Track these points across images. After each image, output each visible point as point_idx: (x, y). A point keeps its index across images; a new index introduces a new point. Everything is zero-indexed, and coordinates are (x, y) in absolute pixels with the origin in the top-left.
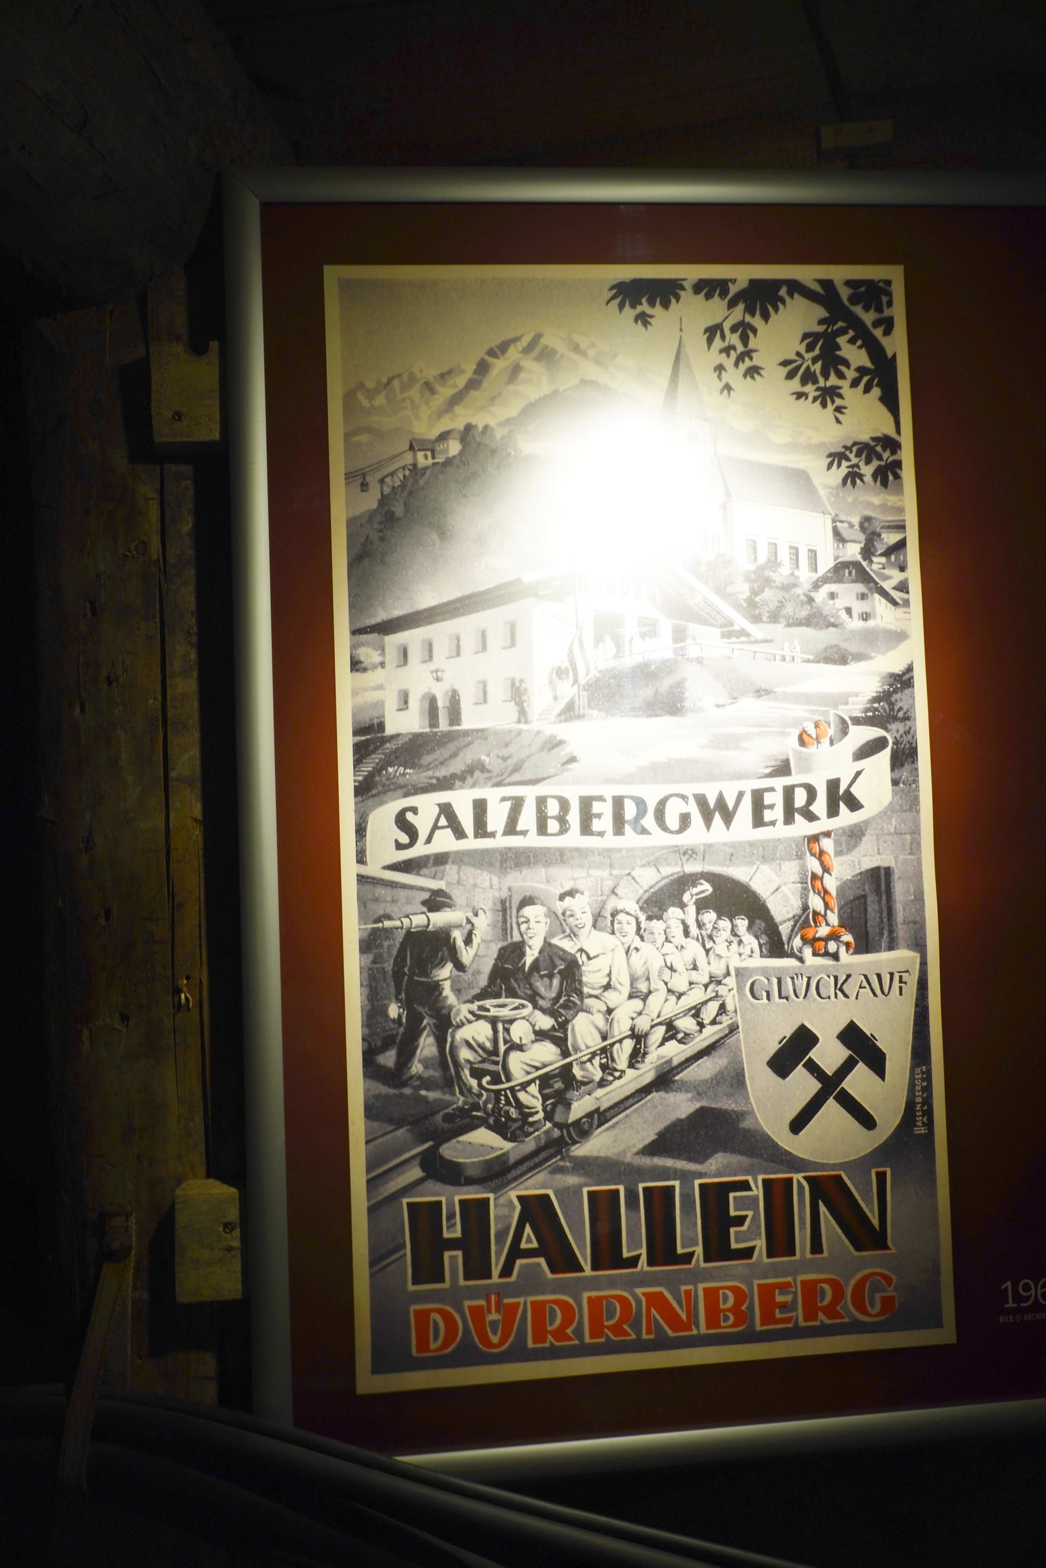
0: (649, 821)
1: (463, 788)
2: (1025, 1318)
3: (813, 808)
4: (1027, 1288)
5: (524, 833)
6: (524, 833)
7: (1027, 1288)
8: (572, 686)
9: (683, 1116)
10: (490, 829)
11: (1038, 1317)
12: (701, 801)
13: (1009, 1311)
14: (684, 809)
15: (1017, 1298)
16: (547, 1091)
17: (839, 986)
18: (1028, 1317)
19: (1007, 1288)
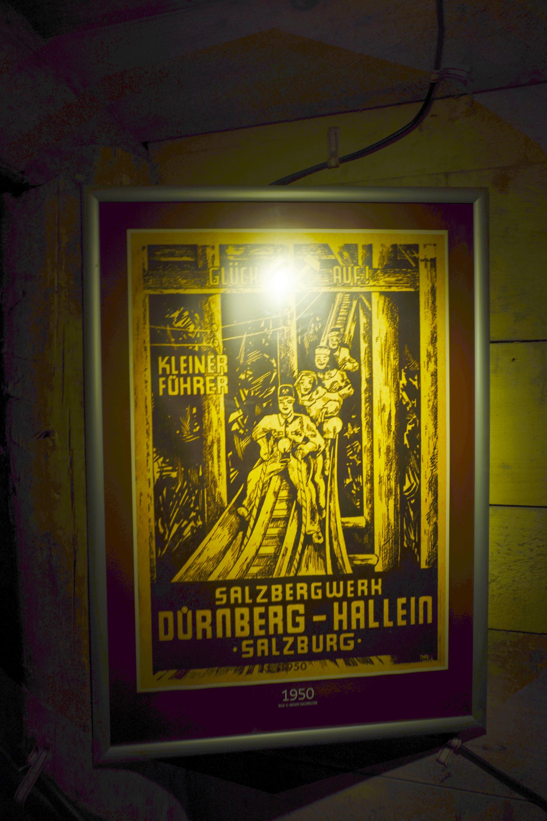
2: (290, 705)
4: (294, 693)
7: (294, 693)
13: (285, 703)
15: (289, 697)
19: (284, 694)
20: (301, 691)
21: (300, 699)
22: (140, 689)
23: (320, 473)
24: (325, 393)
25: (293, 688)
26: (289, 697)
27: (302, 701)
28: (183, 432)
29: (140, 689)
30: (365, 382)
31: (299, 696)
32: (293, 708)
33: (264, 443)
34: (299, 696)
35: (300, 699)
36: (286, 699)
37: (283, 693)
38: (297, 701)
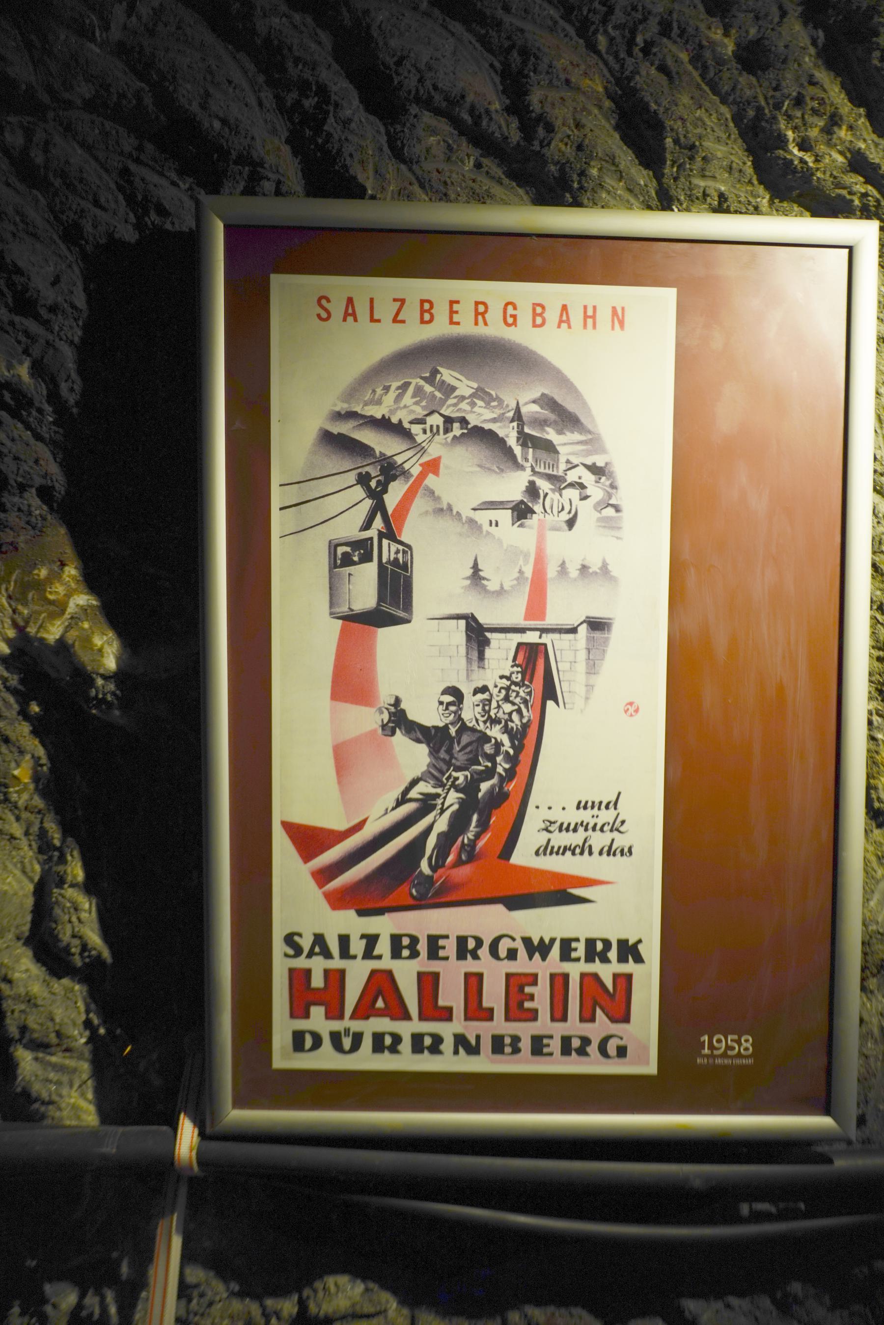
0: (484, 952)
1: (871, 609)
2: (716, 1061)
3: (479, 952)
4: (719, 1041)
5: (379, 957)
6: (379, 957)
7: (719, 1041)
8: (531, 958)
9: (392, 483)
10: (352, 952)
11: (726, 1061)
12: (527, 941)
13: (707, 1056)
14: (512, 945)
15: (711, 1047)
16: (706, 81)
17: (418, 903)
18: (719, 1061)
19: (704, 1041)
20: (732, 1040)
21: (730, 1053)
22: (276, 280)
23: (463, 650)
24: (364, 499)
25: (749, 1034)
26: (711, 1047)
27: (732, 1057)
28: (57, 936)
29: (276, 280)
30: (881, 139)
31: (728, 1048)
32: (720, 1066)
33: (380, 27)
34: (728, 1048)
35: (730, 1053)
36: (706, 1051)
37: (702, 1039)
38: (724, 1055)
